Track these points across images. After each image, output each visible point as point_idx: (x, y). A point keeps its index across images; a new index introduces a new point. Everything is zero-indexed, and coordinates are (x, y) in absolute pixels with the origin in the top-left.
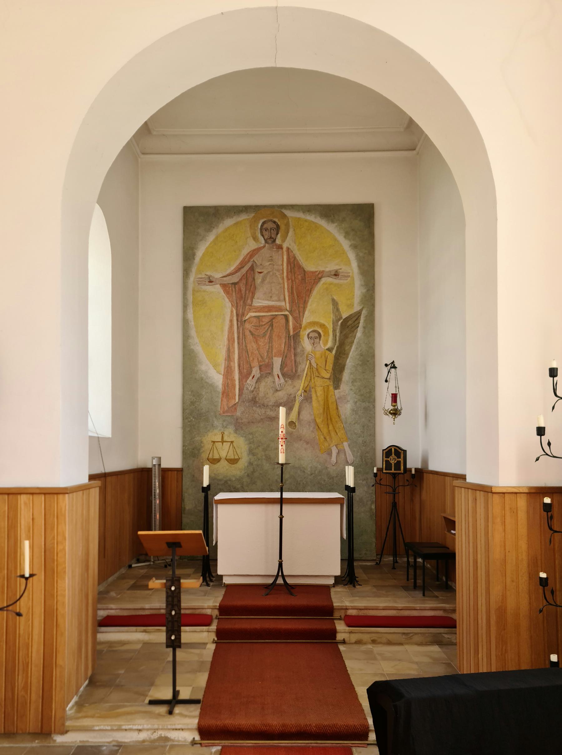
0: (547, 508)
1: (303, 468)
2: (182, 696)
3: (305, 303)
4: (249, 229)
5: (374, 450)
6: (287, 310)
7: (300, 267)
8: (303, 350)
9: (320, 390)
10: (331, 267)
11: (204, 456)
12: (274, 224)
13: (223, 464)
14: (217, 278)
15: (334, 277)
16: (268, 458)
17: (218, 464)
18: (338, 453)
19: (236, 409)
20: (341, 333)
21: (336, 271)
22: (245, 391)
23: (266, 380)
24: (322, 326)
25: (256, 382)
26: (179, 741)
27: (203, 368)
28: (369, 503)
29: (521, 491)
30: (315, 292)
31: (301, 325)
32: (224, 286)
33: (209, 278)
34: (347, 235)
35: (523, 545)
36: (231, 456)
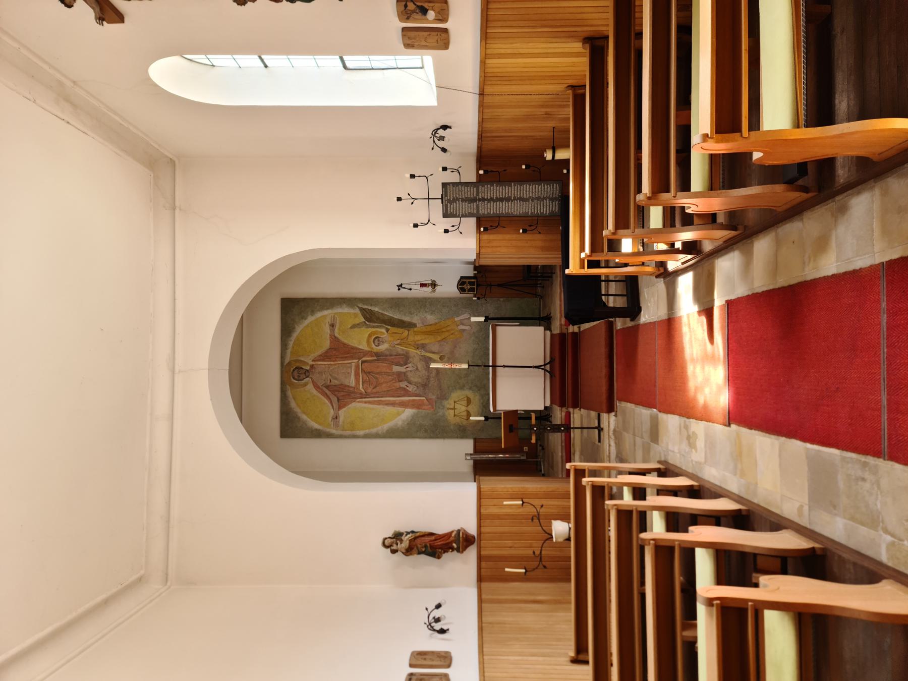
0: (486, 229)
1: (474, 350)
2: (596, 425)
3: (353, 348)
4: (298, 390)
5: (460, 298)
6: (358, 362)
7: (327, 352)
8: (387, 349)
9: (418, 338)
10: (327, 329)
11: (465, 422)
12: (295, 371)
13: (470, 408)
14: (334, 413)
15: (334, 326)
16: (467, 375)
17: (470, 412)
18: (463, 324)
19: (431, 399)
20: (375, 322)
21: (330, 325)
22: (417, 392)
23: (409, 377)
24: (370, 336)
25: (411, 384)
26: (615, 424)
27: (400, 423)
28: (499, 302)
29: (478, 237)
30: (346, 341)
31: (369, 351)
32: (340, 408)
33: (333, 419)
34: (304, 318)
35: (508, 237)
36: (465, 403)
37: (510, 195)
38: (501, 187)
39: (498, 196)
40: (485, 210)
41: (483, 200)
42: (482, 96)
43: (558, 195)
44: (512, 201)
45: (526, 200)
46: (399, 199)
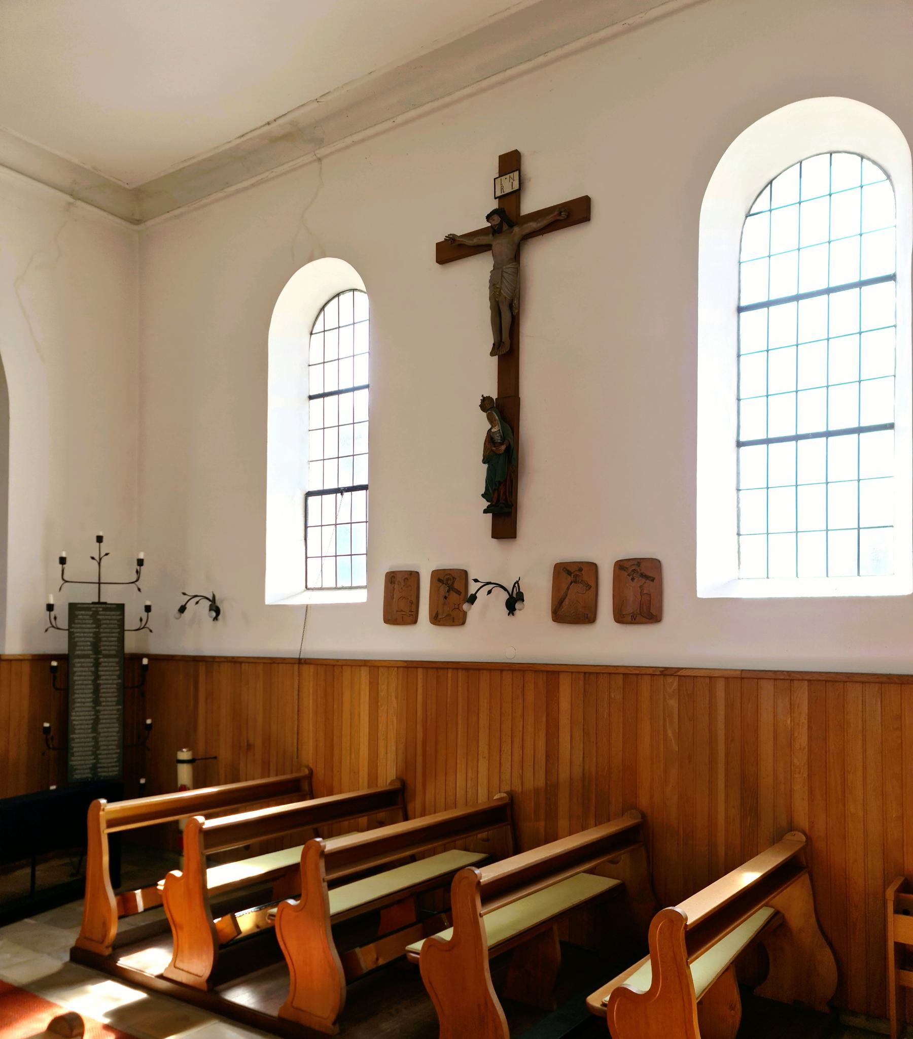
37: (104, 704)
38: (115, 690)
39: (102, 687)
40: (81, 667)
41: (97, 664)
42: (297, 662)
43: (101, 776)
44: (94, 708)
45: (95, 728)
46: (100, 539)
